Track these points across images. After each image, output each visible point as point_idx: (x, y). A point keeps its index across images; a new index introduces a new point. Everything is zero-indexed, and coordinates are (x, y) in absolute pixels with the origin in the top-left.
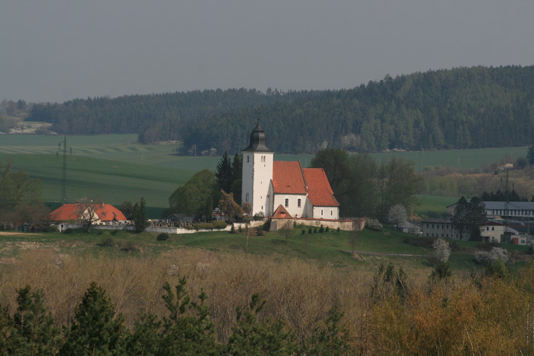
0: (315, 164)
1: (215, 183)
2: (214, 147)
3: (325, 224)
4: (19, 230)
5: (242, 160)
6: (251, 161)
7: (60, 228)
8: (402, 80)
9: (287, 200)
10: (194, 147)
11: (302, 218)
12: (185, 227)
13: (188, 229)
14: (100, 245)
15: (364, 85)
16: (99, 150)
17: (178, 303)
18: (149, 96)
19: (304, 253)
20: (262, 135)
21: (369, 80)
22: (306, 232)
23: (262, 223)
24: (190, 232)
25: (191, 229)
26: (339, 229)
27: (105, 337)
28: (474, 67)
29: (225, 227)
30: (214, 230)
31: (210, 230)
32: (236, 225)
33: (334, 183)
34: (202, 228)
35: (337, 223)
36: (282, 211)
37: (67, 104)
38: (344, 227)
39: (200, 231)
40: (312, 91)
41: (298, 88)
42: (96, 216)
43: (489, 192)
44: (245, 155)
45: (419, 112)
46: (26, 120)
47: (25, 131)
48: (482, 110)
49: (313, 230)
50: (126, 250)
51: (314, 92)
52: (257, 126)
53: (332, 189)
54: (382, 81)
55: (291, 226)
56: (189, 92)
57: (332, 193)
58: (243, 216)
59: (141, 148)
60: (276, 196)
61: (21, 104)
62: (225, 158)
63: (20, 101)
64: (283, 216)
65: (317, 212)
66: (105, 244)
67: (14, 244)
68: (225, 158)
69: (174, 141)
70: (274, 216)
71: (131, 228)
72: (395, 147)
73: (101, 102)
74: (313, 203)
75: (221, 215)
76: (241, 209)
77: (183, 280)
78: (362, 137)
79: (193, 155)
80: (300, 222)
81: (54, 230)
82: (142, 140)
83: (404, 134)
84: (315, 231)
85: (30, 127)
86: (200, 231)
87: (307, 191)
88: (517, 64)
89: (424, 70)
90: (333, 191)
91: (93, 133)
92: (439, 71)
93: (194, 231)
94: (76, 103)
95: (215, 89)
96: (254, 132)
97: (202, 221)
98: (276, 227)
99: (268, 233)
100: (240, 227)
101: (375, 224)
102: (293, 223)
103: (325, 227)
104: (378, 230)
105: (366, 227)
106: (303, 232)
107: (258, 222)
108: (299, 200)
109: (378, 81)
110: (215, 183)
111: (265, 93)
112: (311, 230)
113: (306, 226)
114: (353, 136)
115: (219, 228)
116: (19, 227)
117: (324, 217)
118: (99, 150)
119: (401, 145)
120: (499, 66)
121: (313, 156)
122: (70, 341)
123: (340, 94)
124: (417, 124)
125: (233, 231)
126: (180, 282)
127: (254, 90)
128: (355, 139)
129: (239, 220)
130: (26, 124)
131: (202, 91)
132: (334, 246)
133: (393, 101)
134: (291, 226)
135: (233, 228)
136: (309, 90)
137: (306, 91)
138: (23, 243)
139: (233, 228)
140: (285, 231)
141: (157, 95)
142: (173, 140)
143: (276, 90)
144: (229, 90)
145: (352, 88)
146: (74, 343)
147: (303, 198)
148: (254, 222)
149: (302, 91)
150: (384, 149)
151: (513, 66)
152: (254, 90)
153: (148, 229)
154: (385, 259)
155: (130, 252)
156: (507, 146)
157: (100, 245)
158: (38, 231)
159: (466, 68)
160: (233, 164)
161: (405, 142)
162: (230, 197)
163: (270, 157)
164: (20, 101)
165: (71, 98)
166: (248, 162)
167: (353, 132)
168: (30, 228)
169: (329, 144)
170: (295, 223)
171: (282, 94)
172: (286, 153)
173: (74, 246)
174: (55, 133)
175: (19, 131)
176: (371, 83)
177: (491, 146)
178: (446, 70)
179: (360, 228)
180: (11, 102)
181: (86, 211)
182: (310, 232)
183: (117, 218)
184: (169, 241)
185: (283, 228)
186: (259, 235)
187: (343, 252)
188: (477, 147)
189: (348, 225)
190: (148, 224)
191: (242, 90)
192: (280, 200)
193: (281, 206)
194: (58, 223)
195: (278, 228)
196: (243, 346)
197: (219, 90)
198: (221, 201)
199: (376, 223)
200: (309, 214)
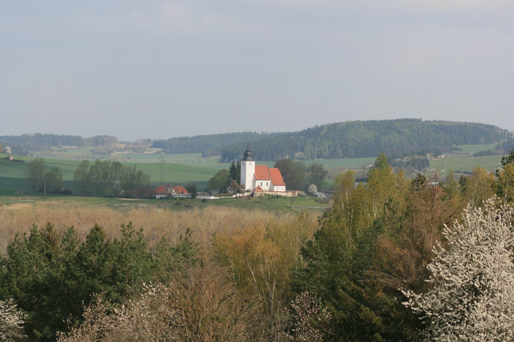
0: (276, 166)
1: (229, 175)
2: (236, 159)
3: (279, 194)
4: (139, 198)
5: (241, 165)
6: (244, 165)
7: (157, 197)
8: (323, 127)
9: (261, 183)
10: (227, 159)
11: (268, 191)
12: (214, 196)
13: (216, 196)
14: (176, 205)
15: (305, 130)
16: (184, 161)
17: (127, 233)
18: (207, 135)
19: (269, 207)
20: (249, 153)
21: (307, 127)
22: (270, 198)
23: (250, 193)
24: (217, 198)
25: (217, 197)
26: (285, 196)
27: (97, 249)
28: (356, 121)
29: (233, 196)
30: (228, 197)
31: (226, 197)
32: (238, 195)
33: (283, 175)
34: (222, 196)
35: (285, 193)
36: (259, 188)
37: (169, 140)
38: (288, 195)
39: (221, 197)
40: (282, 133)
41: (276, 131)
42: (174, 191)
43: (359, 178)
44: (242, 162)
45: (331, 141)
46: (151, 147)
47: (151, 152)
48: (359, 141)
49: (273, 196)
50: (187, 207)
51: (283, 133)
52: (247, 149)
53: (283, 177)
54: (313, 128)
55: (263, 195)
56: (225, 134)
57: (282, 179)
58: (241, 191)
59: (203, 160)
60: (256, 181)
61: (149, 140)
62: (233, 164)
63: (148, 139)
64: (260, 190)
65: (276, 188)
66: (178, 204)
67: (136, 205)
68: (233, 164)
69: (218, 156)
70: (256, 190)
71: (190, 197)
72: (319, 158)
73: (185, 139)
74: (274, 184)
75: (231, 190)
76: (240, 187)
77: (131, 222)
78: (304, 154)
79: (227, 163)
80: (267, 193)
81: (155, 198)
82: (204, 156)
83: (324, 152)
84: (274, 197)
85: (153, 151)
86: (221, 197)
87: (271, 179)
88: (375, 119)
89: (333, 122)
90: (283, 178)
91: (181, 153)
92: (339, 123)
93: (218, 198)
94: (174, 139)
95: (237, 132)
96: (246, 152)
97: (223, 193)
98: (256, 195)
99: (253, 198)
100: (240, 196)
101: (302, 193)
102: (264, 194)
103: (279, 195)
104: (303, 196)
105: (298, 195)
106: (269, 198)
107: (248, 193)
108: (267, 183)
109: (312, 128)
110: (229, 175)
111: (261, 134)
112: (273, 197)
113: (271, 195)
114: (300, 153)
115: (230, 196)
116: (138, 197)
117: (278, 190)
118: (184, 161)
119: (322, 157)
120: (367, 120)
121: (274, 163)
122: (81, 251)
123: (294, 134)
124: (329, 147)
125: (236, 198)
126: (130, 223)
127: (256, 132)
128: (301, 154)
129: (239, 192)
130: (151, 149)
131: (231, 133)
132: (283, 203)
133: (319, 137)
134: (263, 195)
135: (236, 196)
136: (281, 132)
137: (279, 133)
138: (140, 204)
139: (236, 196)
140: (260, 197)
141: (211, 135)
142: (218, 155)
143: (266, 132)
144: (244, 132)
145: (300, 131)
146: (83, 252)
147: (269, 182)
148: (246, 193)
149: (278, 133)
150: (315, 159)
151: (63, 135)
152: (256, 132)
153: (197, 197)
154: (307, 209)
155: (189, 207)
156: (371, 157)
157: (176, 205)
158: (148, 198)
159: (352, 121)
160: (237, 167)
161: (324, 155)
162: (235, 182)
163: (253, 163)
164: (148, 139)
165: (171, 137)
166: (243, 165)
167: (300, 151)
168: (144, 197)
169: (289, 157)
170: (265, 194)
171: (268, 134)
172: (269, 161)
173: (163, 205)
174: (164, 153)
175: (148, 153)
176: (308, 128)
177: (363, 157)
178: (343, 122)
179: (295, 195)
180: (144, 139)
181: (169, 189)
182: (272, 197)
183: (183, 192)
184: (207, 203)
185: (260, 196)
186: (249, 199)
187: (287, 207)
188: (357, 157)
189: (290, 194)
190: (198, 195)
191: (250, 132)
192: (258, 183)
193: (259, 186)
194: (157, 194)
195: (257, 196)
196: (161, 253)
197: (239, 133)
198: (231, 184)
199: (303, 193)
200: (272, 189)
